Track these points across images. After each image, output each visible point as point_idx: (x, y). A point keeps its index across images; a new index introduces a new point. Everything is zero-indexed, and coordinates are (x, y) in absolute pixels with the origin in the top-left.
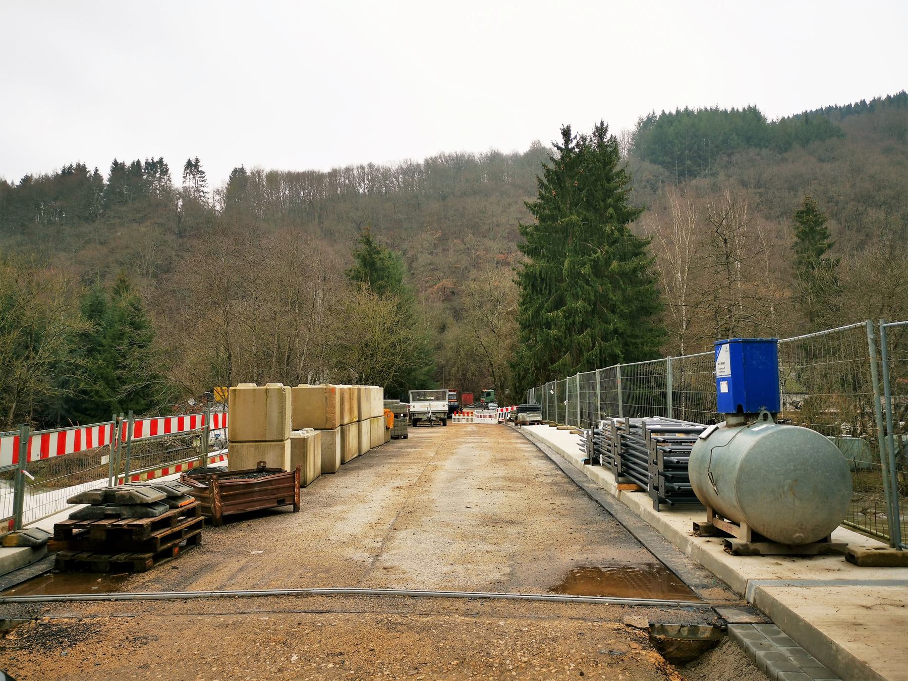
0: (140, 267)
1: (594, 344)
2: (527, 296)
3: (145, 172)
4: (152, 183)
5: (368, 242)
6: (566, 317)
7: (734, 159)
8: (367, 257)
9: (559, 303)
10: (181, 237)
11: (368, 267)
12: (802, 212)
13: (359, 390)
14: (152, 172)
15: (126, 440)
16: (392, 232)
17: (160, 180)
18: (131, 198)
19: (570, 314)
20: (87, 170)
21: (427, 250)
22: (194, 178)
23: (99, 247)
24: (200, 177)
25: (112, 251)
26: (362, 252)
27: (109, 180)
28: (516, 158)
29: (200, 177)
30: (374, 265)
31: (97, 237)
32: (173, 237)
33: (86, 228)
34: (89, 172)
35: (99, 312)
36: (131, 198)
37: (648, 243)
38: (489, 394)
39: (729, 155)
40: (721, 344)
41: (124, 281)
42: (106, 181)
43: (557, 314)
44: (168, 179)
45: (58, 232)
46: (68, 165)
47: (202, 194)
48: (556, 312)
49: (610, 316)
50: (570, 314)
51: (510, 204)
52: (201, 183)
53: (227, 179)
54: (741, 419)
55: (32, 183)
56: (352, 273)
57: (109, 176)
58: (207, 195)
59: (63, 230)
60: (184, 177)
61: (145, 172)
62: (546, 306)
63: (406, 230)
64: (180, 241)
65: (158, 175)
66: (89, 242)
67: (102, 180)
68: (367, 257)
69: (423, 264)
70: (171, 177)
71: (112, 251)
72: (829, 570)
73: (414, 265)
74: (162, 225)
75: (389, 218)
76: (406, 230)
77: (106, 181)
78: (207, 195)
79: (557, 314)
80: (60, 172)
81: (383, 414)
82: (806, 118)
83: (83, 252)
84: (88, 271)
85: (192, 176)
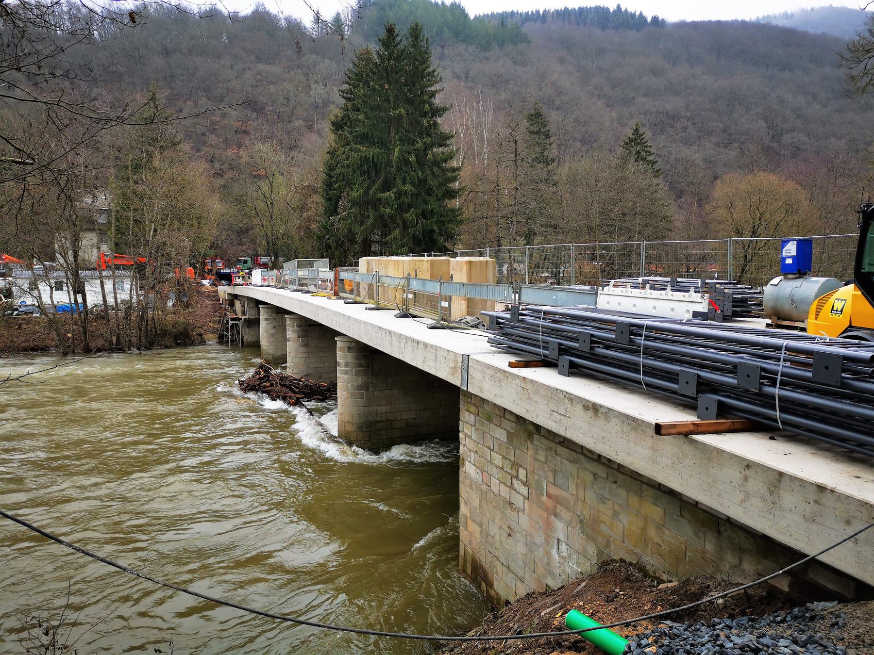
1: (417, 221)
2: (340, 175)
6: (397, 199)
7: (446, 51)
9: (387, 186)
12: (532, 115)
15: (679, 280)
19: (400, 195)
28: (234, 18)
37: (452, 137)
38: (246, 262)
39: (443, 47)
40: (789, 241)
44: (167, 53)
48: (388, 193)
49: (429, 199)
50: (400, 195)
51: (244, 70)
54: (798, 276)
82: (503, 18)
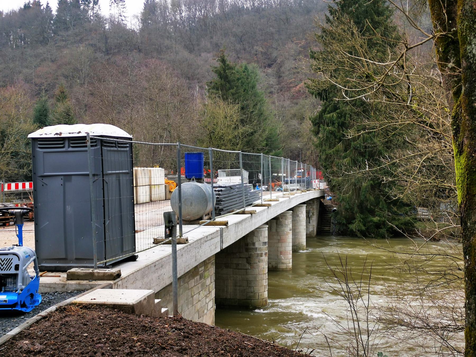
0: (79, 78)
3: (82, 4)
4: (87, 11)
5: (223, 61)
6: (338, 117)
8: (222, 72)
10: (108, 54)
11: (223, 80)
13: (150, 170)
14: (87, 3)
16: (266, 43)
17: (93, 9)
18: (72, 25)
20: (41, 4)
21: (292, 56)
22: (117, 6)
23: (50, 64)
24: (122, 5)
25: (59, 67)
26: (219, 68)
27: (58, 11)
29: (122, 5)
30: (227, 78)
31: (49, 56)
32: (101, 55)
33: (41, 50)
34: (42, 5)
35: (45, 116)
36: (72, 25)
41: (63, 92)
42: (54, 12)
43: (333, 115)
45: (22, 53)
46: (27, 2)
47: (123, 18)
52: (123, 10)
53: (142, 6)
55: (4, 16)
56: (213, 85)
57: (57, 8)
58: (127, 19)
59: (26, 51)
60: (110, 6)
61: (82, 4)
62: (328, 109)
63: (277, 41)
64: (107, 57)
65: (91, 5)
66: (44, 60)
67: (52, 11)
68: (222, 72)
69: (288, 68)
70: (100, 6)
71: (59, 67)
72: (390, 265)
73: (282, 69)
74: (95, 45)
75: (264, 32)
76: (277, 41)
77: (54, 12)
78: (127, 19)
79: (333, 115)
80: (23, 7)
81: (164, 183)
83: (39, 69)
84: (44, 83)
85: (116, 4)
